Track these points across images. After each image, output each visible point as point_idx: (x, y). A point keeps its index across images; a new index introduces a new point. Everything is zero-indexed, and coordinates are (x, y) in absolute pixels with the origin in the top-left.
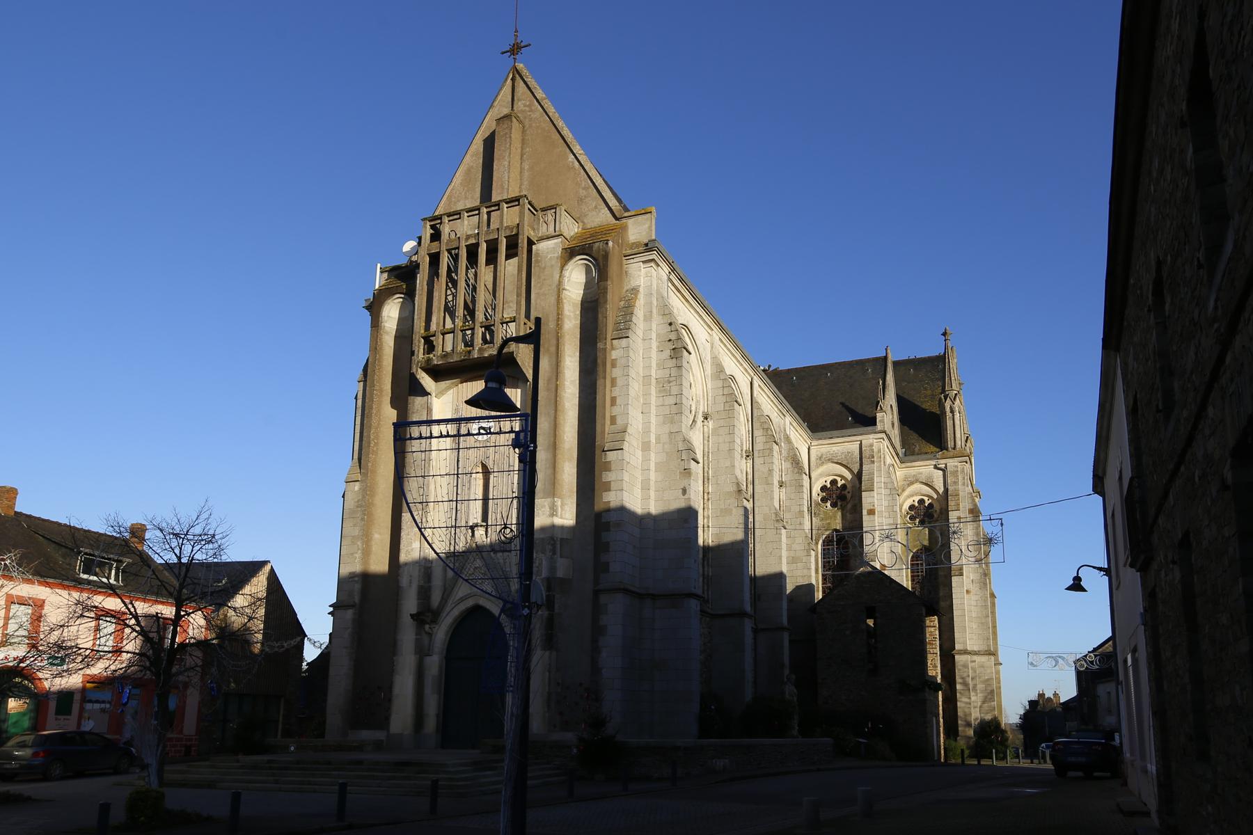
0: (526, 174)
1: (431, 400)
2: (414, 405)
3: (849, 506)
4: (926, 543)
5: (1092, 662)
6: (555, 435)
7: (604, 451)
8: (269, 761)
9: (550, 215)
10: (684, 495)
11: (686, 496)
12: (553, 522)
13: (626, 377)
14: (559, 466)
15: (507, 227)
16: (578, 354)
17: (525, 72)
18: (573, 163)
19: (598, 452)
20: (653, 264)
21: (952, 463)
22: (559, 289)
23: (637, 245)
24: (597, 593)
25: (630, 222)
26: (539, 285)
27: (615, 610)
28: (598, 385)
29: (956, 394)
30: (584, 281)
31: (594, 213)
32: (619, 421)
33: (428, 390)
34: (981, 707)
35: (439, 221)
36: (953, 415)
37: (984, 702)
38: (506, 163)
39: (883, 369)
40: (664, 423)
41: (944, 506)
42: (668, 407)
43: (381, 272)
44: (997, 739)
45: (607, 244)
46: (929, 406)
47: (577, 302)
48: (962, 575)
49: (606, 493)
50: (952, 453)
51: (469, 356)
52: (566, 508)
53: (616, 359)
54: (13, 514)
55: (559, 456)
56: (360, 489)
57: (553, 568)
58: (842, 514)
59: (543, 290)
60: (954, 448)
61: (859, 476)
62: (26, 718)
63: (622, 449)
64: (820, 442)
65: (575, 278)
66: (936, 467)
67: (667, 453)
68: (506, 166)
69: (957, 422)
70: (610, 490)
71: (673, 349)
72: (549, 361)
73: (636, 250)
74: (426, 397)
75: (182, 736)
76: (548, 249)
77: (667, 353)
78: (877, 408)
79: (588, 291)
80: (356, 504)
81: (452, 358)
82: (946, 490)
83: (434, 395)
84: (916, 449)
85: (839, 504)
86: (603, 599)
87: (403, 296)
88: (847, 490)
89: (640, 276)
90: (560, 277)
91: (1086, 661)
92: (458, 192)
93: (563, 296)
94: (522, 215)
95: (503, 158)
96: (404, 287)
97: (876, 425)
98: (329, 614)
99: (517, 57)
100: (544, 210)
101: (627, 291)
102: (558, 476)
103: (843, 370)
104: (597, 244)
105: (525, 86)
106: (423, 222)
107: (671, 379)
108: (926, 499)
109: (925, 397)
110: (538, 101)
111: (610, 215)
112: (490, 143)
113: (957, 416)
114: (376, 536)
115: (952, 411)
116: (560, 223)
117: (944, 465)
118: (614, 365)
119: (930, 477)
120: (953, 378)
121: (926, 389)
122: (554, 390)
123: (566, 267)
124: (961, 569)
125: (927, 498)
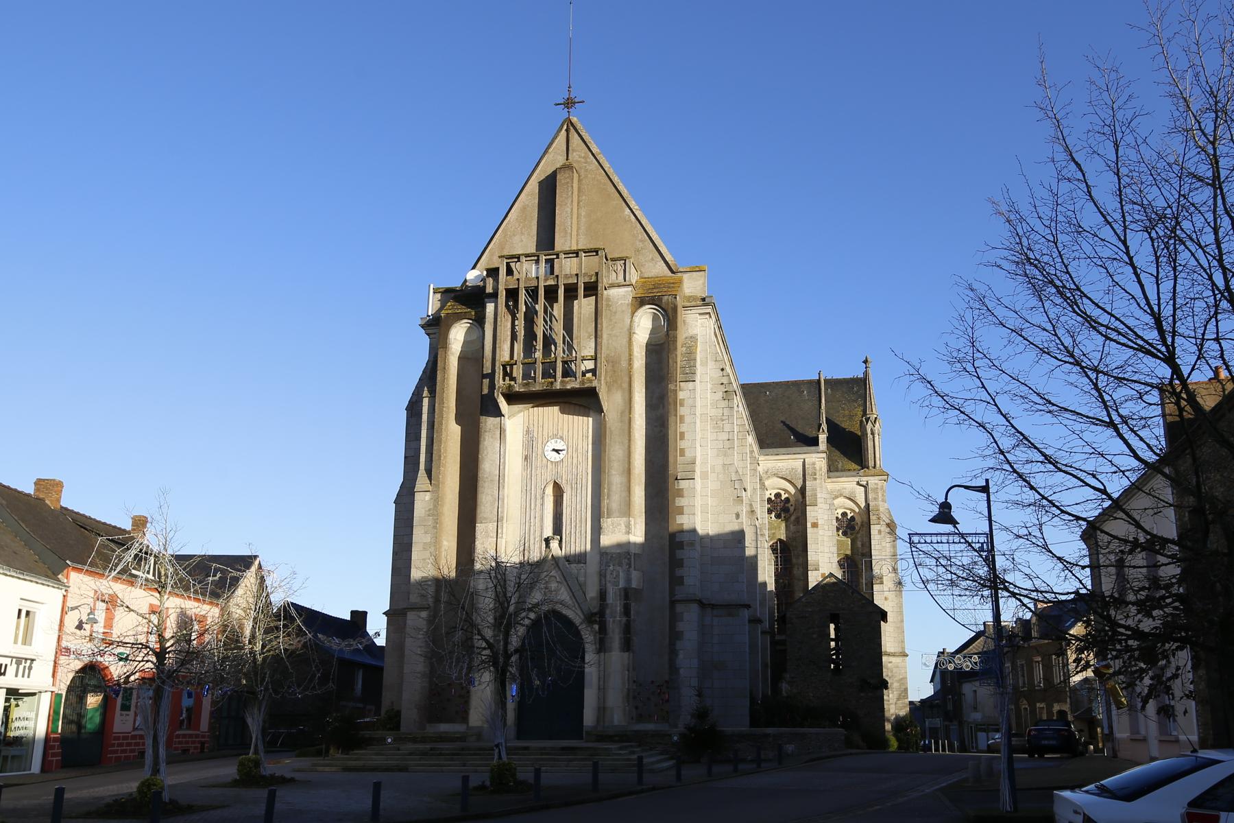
0: (583, 220)
1: (504, 421)
2: (485, 425)
3: (793, 518)
4: (849, 552)
5: (976, 663)
6: (629, 463)
7: (676, 479)
8: (431, 749)
9: (619, 266)
10: (737, 519)
11: (739, 520)
12: (629, 539)
13: (694, 416)
14: (632, 489)
15: (585, 274)
16: (644, 390)
17: (579, 126)
18: (629, 217)
19: (671, 480)
20: (707, 316)
21: (873, 481)
22: (630, 333)
23: (694, 298)
24: (673, 603)
25: (686, 276)
26: (610, 327)
27: (690, 618)
28: (669, 421)
29: (876, 418)
30: (651, 327)
31: (651, 264)
32: (687, 453)
33: (503, 412)
34: (896, 704)
35: (516, 260)
36: (874, 437)
37: (898, 699)
38: (569, 210)
39: (817, 392)
40: (718, 455)
41: (865, 520)
42: (721, 442)
43: (434, 293)
44: (912, 732)
45: (676, 298)
46: (852, 426)
47: (642, 344)
48: (883, 584)
49: (680, 516)
50: (872, 471)
51: (552, 387)
52: (638, 526)
53: (684, 399)
54: (59, 507)
55: (632, 481)
56: (431, 499)
57: (629, 580)
58: (786, 525)
59: (615, 332)
60: (874, 467)
61: (802, 491)
62: (98, 714)
63: (694, 479)
64: (767, 457)
65: (644, 323)
66: (858, 484)
67: (721, 482)
68: (569, 212)
69: (877, 443)
70: (683, 514)
71: (726, 392)
72: (622, 396)
73: (693, 303)
74: (498, 419)
75: (198, 732)
76: (619, 296)
77: (720, 395)
78: (819, 430)
79: (653, 336)
80: (427, 513)
81: (535, 388)
82: (868, 506)
83: (506, 416)
84: (840, 466)
85: (783, 515)
86: (679, 608)
87: (471, 322)
88: (791, 503)
89: (696, 326)
90: (631, 322)
91: (971, 662)
92: (513, 228)
93: (633, 339)
94: (600, 263)
95: (565, 205)
96: (473, 313)
97: (818, 445)
98: (384, 614)
99: (570, 110)
100: (613, 260)
101: (686, 338)
102: (632, 498)
103: (780, 390)
104: (666, 297)
105: (579, 138)
106: (500, 260)
107: (724, 418)
108: (848, 512)
109: (844, 416)
110: (593, 154)
111: (666, 268)
112: (549, 188)
113: (877, 436)
114: (445, 543)
115: (873, 434)
116: (630, 274)
117: (865, 483)
118: (682, 405)
119: (853, 493)
120: (873, 403)
121: (843, 409)
122: (627, 422)
123: (636, 314)
124: (881, 578)
125: (784, 492)
